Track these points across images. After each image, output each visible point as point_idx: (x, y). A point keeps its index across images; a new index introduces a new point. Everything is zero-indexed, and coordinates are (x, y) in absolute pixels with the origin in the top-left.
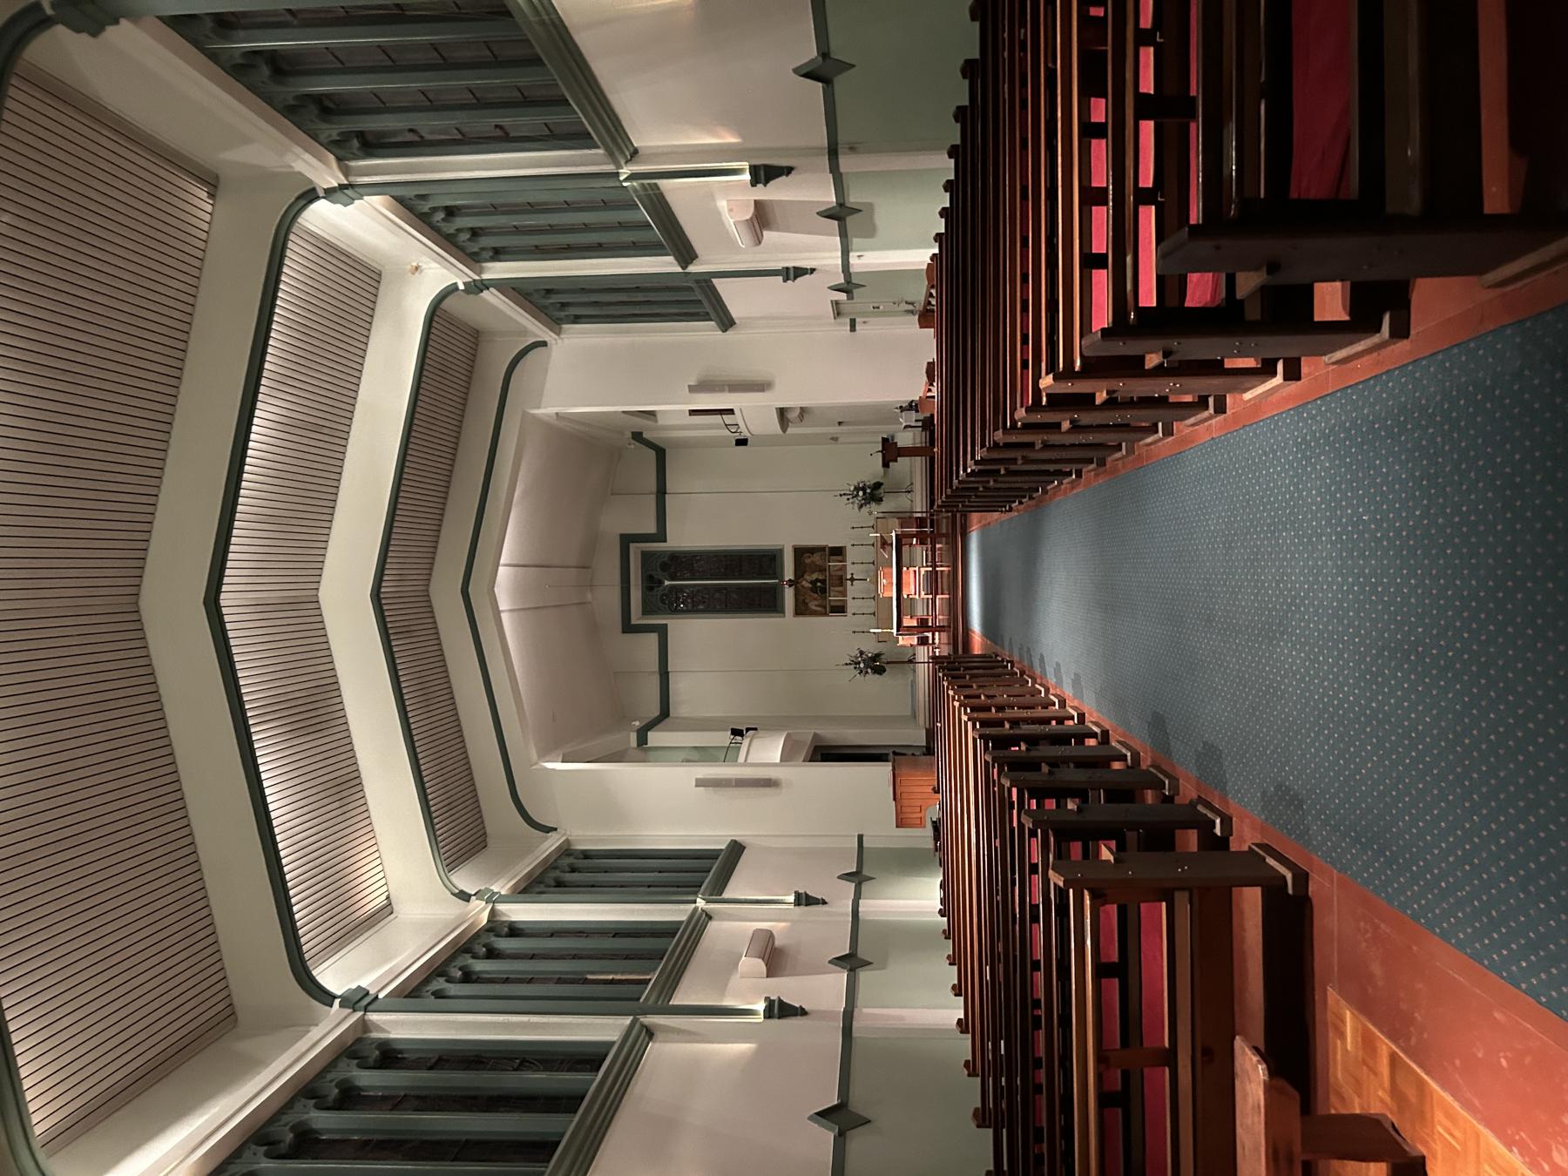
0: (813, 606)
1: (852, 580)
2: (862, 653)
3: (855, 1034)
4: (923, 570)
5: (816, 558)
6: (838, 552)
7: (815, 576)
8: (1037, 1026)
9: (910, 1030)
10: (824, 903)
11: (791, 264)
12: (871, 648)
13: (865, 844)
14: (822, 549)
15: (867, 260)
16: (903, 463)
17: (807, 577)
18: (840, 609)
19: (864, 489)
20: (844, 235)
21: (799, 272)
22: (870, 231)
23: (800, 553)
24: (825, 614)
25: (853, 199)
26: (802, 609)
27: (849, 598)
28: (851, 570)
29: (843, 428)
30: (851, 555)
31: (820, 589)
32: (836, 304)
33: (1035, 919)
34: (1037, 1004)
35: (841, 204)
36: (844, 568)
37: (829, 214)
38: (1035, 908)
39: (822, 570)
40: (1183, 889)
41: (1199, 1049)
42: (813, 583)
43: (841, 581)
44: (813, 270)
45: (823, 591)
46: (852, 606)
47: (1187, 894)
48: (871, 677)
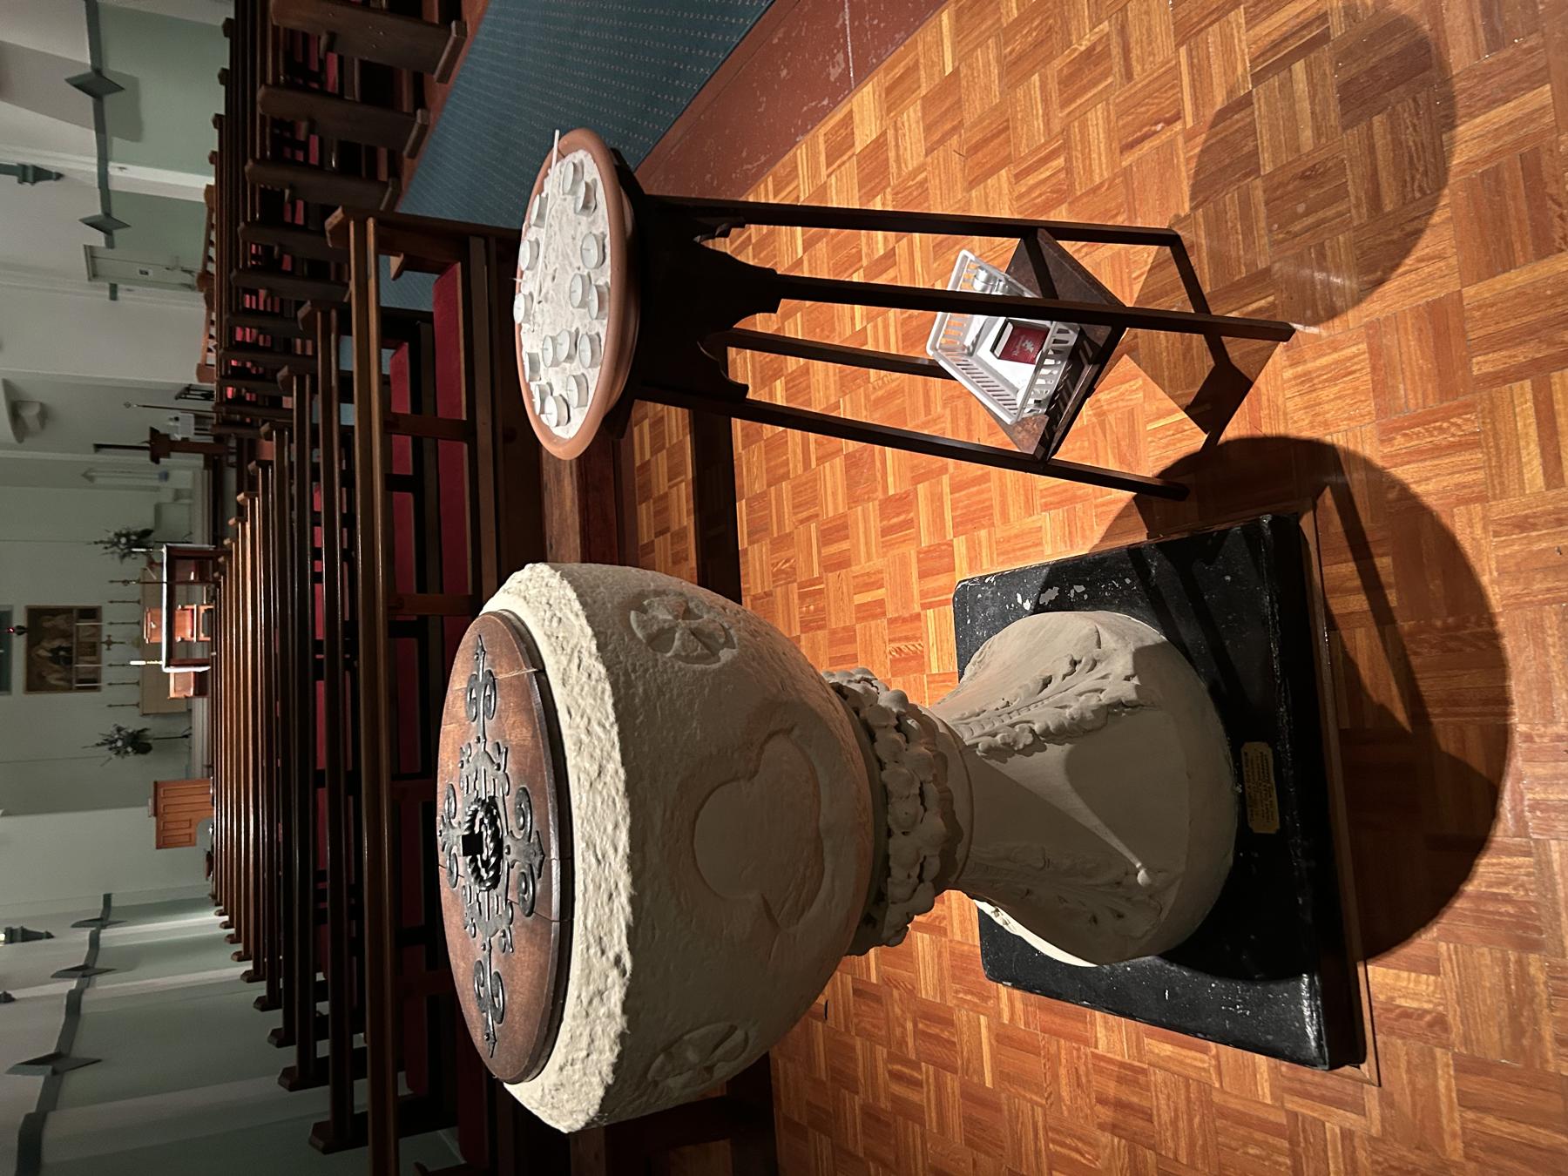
0: (52, 679)
1: (109, 643)
2: (119, 730)
3: (85, 1010)
4: (202, 609)
5: (60, 621)
6: (91, 613)
7: (57, 643)
8: (320, 917)
9: (163, 993)
10: (49, 936)
11: (30, 161)
12: (133, 723)
13: (114, 904)
14: (67, 611)
15: (131, 175)
16: (175, 460)
17: (45, 644)
18: (91, 683)
19: (127, 535)
20: (100, 128)
21: (39, 175)
22: (135, 132)
23: (35, 614)
24: (70, 689)
25: (116, 66)
26: (36, 683)
27: (104, 665)
28: (107, 631)
29: (103, 457)
30: (108, 615)
31: (64, 659)
32: (90, 252)
33: (315, 477)
34: (317, 554)
35: (97, 71)
36: (98, 628)
37: (81, 84)
38: (314, 428)
39: (66, 635)
40: (479, 236)
41: (499, 430)
42: (55, 651)
43: (93, 649)
44: (59, 176)
45: (69, 661)
46: (107, 675)
47: (482, 242)
48: (133, 760)
